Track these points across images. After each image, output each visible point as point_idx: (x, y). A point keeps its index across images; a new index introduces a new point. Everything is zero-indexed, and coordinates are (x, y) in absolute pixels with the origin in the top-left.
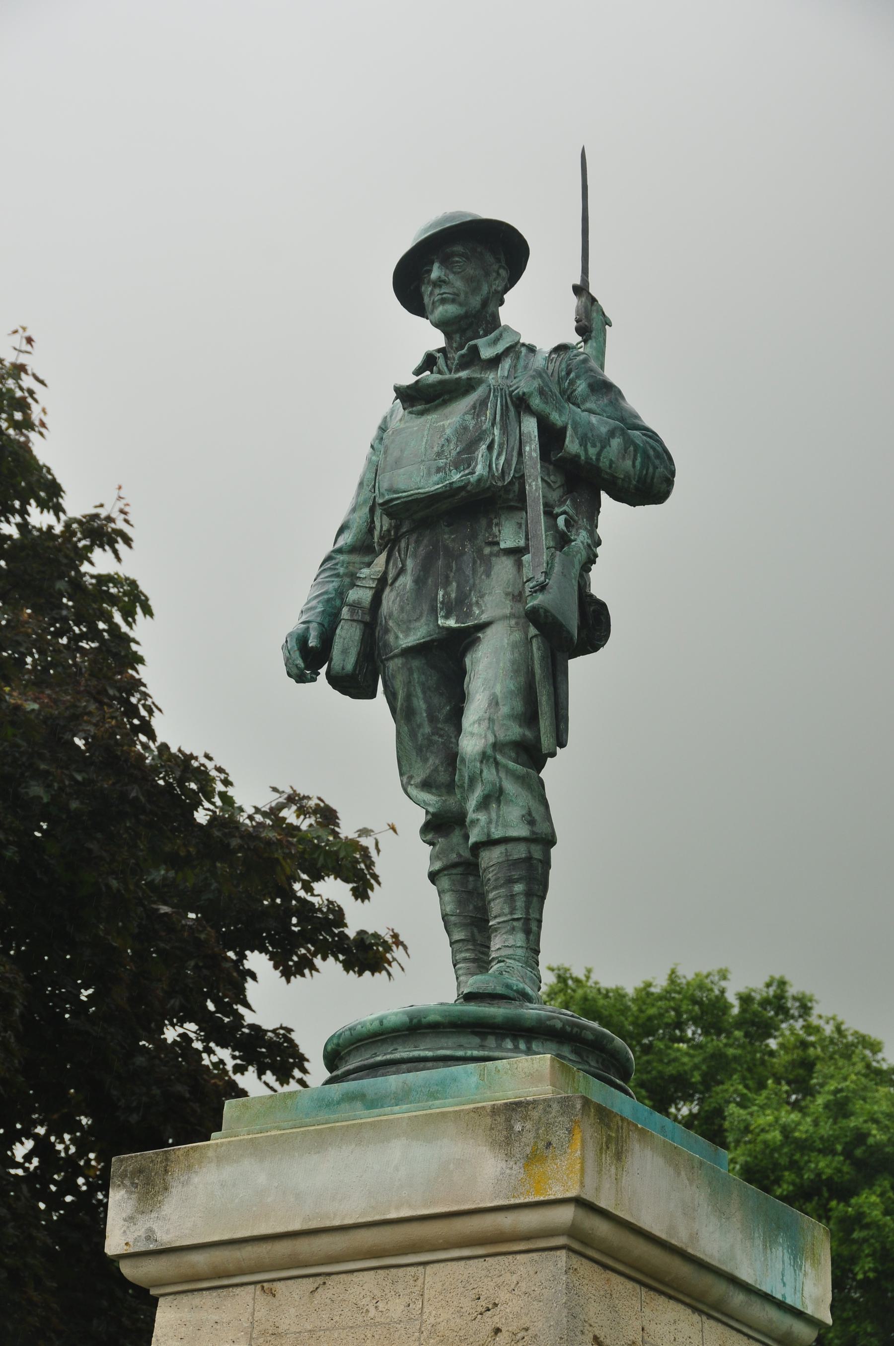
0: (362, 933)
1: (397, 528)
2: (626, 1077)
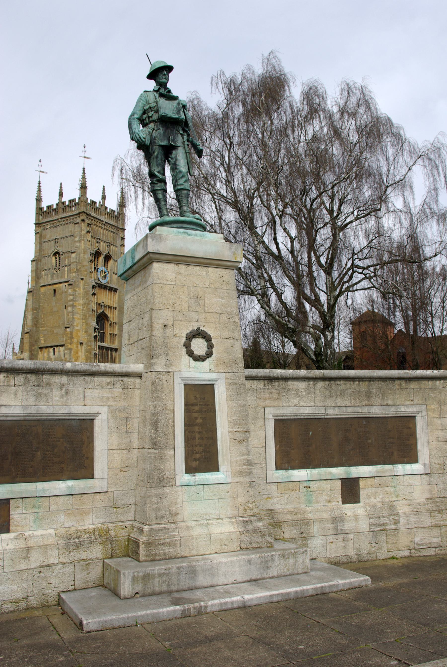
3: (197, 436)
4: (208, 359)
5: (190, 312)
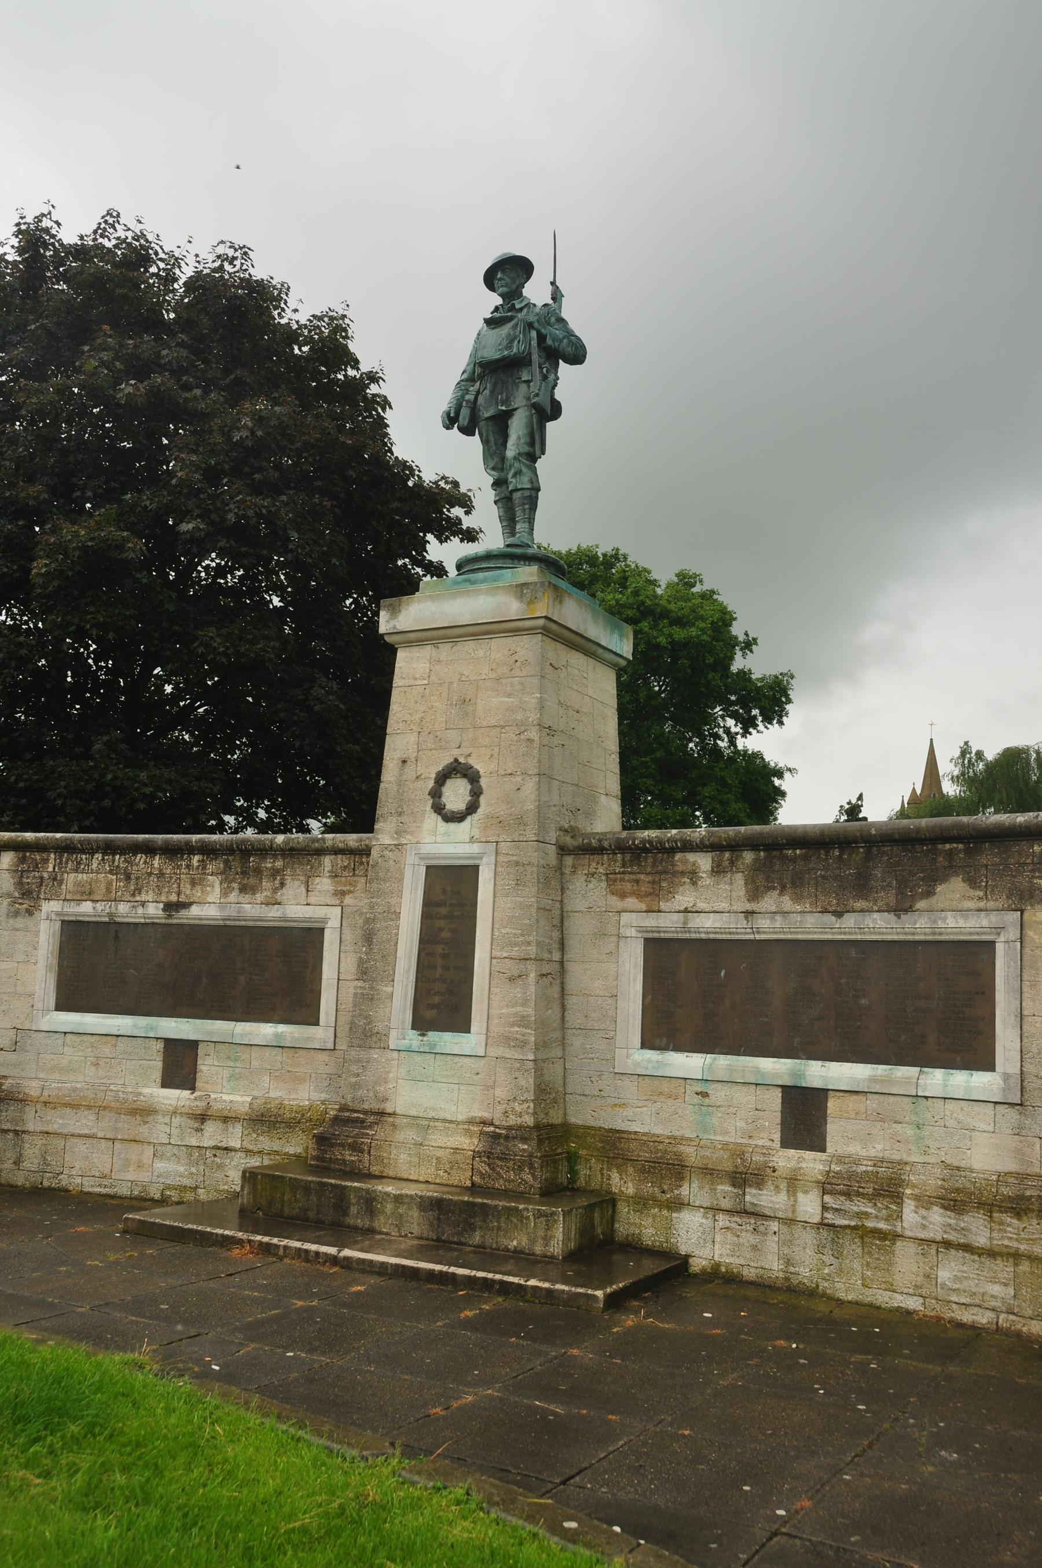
0: (468, 527)
1: (484, 372)
2: (564, 575)
3: (440, 962)
4: (469, 818)
5: (448, 731)
